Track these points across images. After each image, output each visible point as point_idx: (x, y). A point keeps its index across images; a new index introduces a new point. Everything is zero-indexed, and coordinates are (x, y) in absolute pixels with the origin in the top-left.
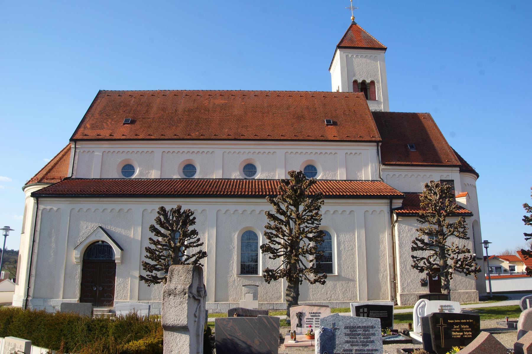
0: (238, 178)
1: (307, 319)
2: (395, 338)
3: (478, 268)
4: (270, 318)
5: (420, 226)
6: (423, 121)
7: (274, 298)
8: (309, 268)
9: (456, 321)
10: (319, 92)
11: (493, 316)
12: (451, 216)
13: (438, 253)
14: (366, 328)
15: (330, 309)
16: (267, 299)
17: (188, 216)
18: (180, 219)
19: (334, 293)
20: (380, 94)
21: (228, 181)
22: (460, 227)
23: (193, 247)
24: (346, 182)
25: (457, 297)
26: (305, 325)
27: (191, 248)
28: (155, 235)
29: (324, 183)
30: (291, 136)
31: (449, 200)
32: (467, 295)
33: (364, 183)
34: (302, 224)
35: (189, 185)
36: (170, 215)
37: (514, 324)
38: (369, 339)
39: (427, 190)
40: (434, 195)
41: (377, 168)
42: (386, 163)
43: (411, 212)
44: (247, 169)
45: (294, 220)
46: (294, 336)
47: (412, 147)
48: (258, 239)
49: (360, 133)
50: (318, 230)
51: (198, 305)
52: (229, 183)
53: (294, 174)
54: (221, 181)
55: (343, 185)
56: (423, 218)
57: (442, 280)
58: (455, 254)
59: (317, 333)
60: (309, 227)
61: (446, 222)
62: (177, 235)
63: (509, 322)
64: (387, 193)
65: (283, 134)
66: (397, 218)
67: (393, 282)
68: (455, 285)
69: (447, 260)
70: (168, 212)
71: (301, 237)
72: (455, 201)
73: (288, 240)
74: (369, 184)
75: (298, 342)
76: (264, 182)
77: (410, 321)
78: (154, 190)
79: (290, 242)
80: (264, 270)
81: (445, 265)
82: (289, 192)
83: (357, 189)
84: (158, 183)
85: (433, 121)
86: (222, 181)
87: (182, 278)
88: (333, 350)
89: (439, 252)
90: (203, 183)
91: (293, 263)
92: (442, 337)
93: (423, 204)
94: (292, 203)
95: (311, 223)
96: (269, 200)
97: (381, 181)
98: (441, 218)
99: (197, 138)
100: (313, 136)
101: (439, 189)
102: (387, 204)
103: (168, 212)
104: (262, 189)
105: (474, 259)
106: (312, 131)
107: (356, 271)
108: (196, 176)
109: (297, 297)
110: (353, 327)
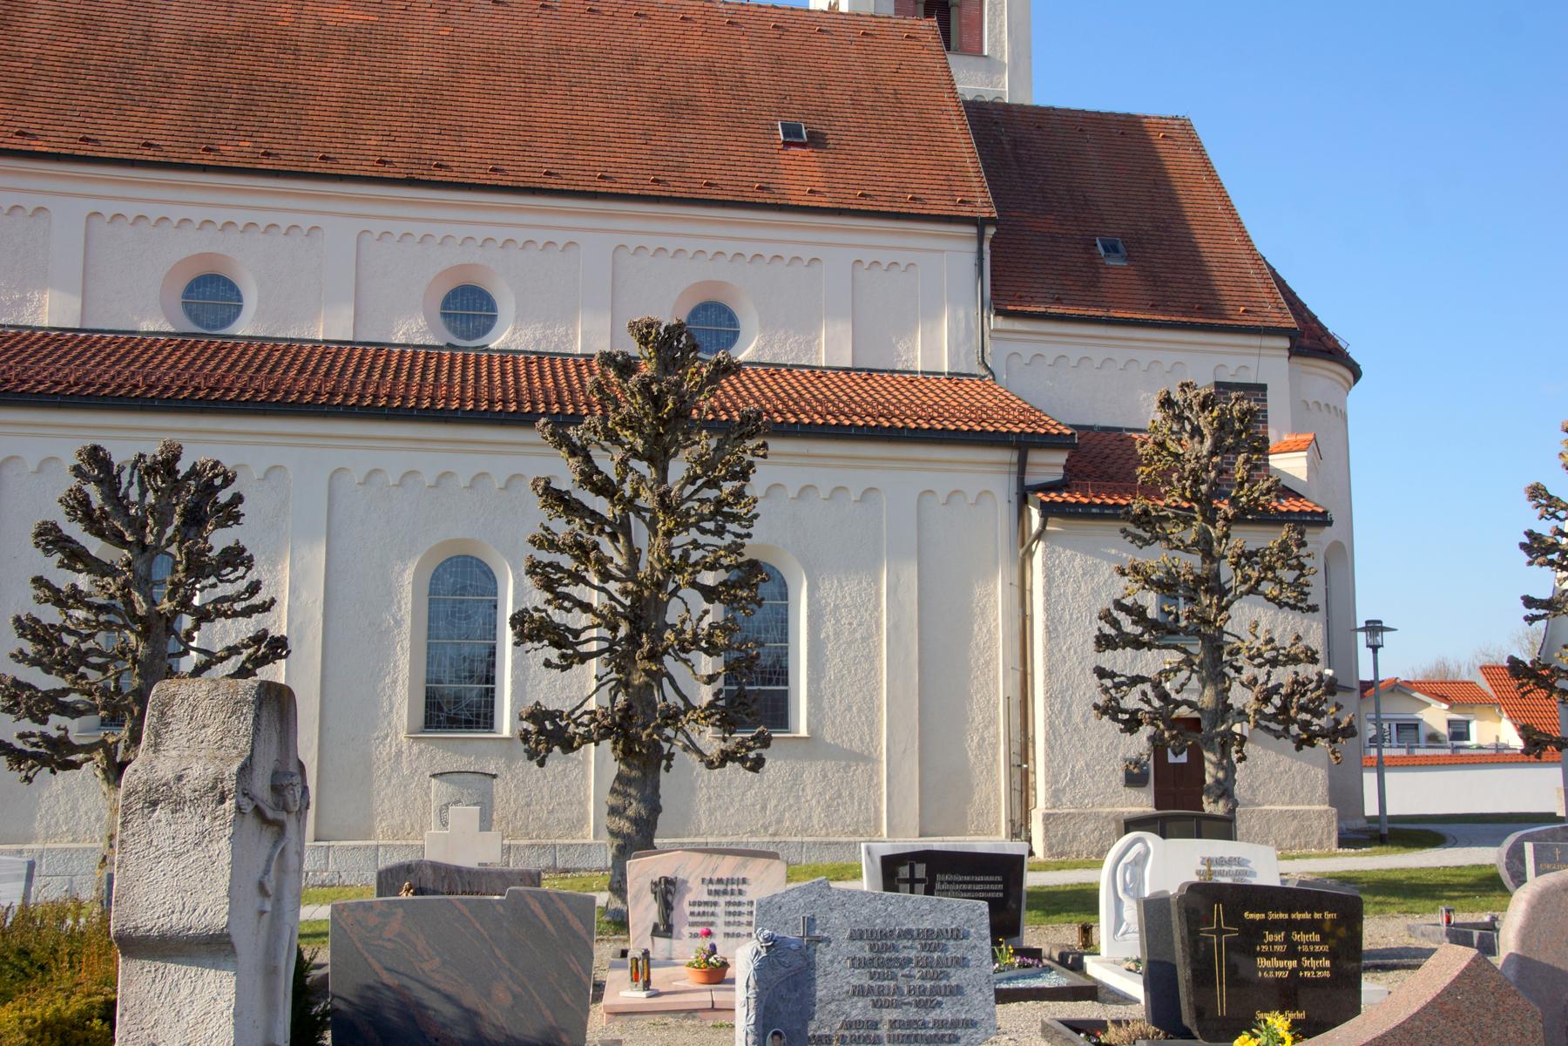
0: (418, 341)
1: (693, 904)
2: (1032, 981)
3: (1344, 724)
4: (554, 897)
5: (1130, 554)
6: (1163, 147)
7: (558, 825)
8: (700, 707)
9: (1272, 916)
10: (759, 6)
11: (1390, 904)
12: (1252, 522)
13: (1197, 661)
14: (932, 939)
15: (785, 865)
16: (531, 828)
17: (209, 490)
18: (174, 501)
19: (791, 806)
20: (1001, 32)
21: (376, 351)
22: (1283, 565)
23: (227, 617)
24: (849, 377)
25: (1257, 828)
26: (687, 927)
27: (220, 623)
28: (59, 567)
29: (765, 376)
30: (638, 181)
31: (1247, 461)
32: (1295, 822)
33: (922, 383)
34: (678, 534)
35: (213, 363)
36: (131, 483)
37: (1472, 933)
38: (944, 982)
39: (1164, 419)
40: (1192, 437)
41: (973, 326)
42: (1010, 308)
43: (1098, 501)
44: (458, 305)
45: (648, 516)
46: (641, 971)
47: (1111, 248)
48: (496, 588)
49: (913, 186)
50: (740, 560)
51: (275, 845)
52: (381, 361)
53: (654, 331)
54: (347, 350)
55: (838, 386)
56: (1147, 525)
57: (1207, 764)
58: (1260, 666)
59: (743, 959)
60: (705, 545)
61: (1232, 543)
62: (161, 570)
63: (1455, 925)
64: (1008, 425)
65: (609, 169)
66: (1044, 525)
67: (1020, 766)
68: (1250, 786)
69: (1228, 689)
70: (121, 469)
71: (671, 586)
72: (1268, 465)
73: (622, 595)
74: (939, 388)
75: (658, 994)
76: (528, 363)
77: (1085, 918)
78: (52, 374)
79: (628, 602)
80: (525, 710)
81: (1220, 706)
82: (632, 405)
83: (893, 405)
84: (71, 350)
85: (1199, 150)
86: (352, 350)
87: (209, 733)
88: (805, 1025)
89: (1202, 655)
90: (269, 355)
91: (640, 687)
92: (1221, 976)
93: (1147, 470)
94: (640, 450)
95: (713, 528)
96: (551, 435)
97: (985, 377)
98: (1215, 527)
99: (246, 166)
100: (728, 188)
101: (1215, 414)
102: (1007, 468)
103: (121, 469)
104: (517, 391)
105: (1332, 687)
106: (723, 167)
107: (880, 722)
108: (243, 327)
109: (651, 818)
110: (884, 935)
